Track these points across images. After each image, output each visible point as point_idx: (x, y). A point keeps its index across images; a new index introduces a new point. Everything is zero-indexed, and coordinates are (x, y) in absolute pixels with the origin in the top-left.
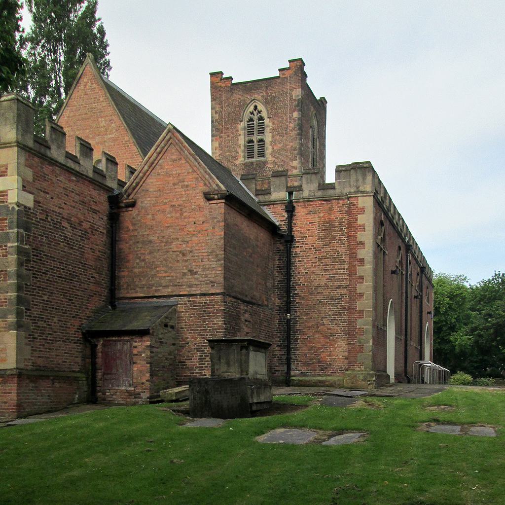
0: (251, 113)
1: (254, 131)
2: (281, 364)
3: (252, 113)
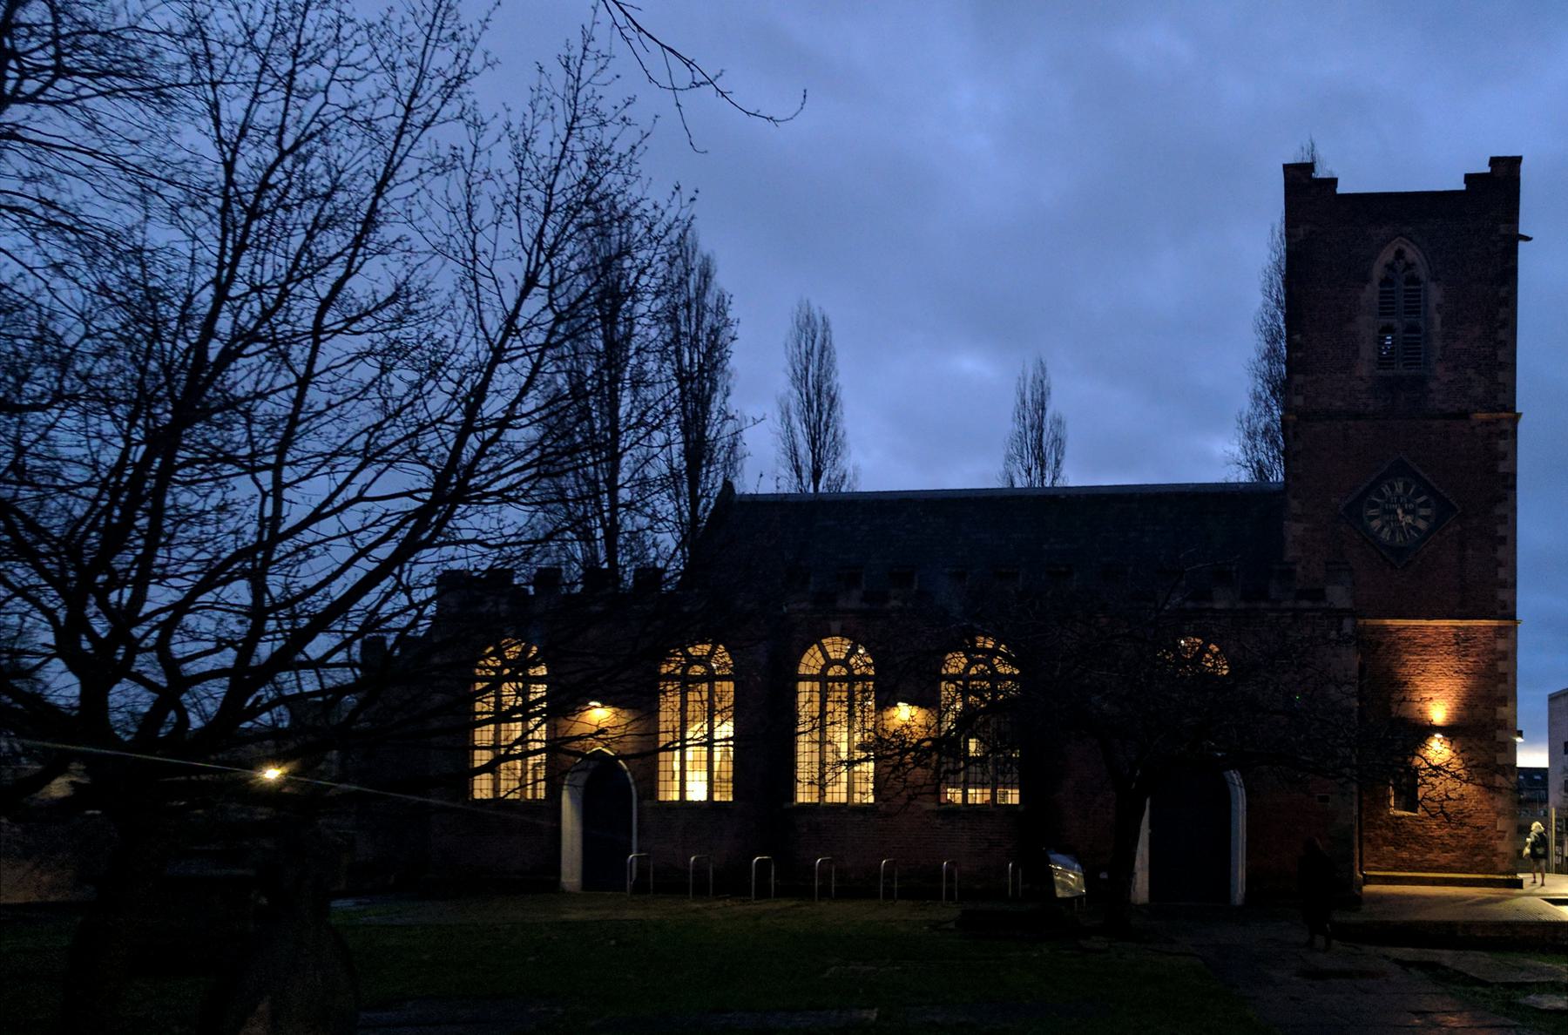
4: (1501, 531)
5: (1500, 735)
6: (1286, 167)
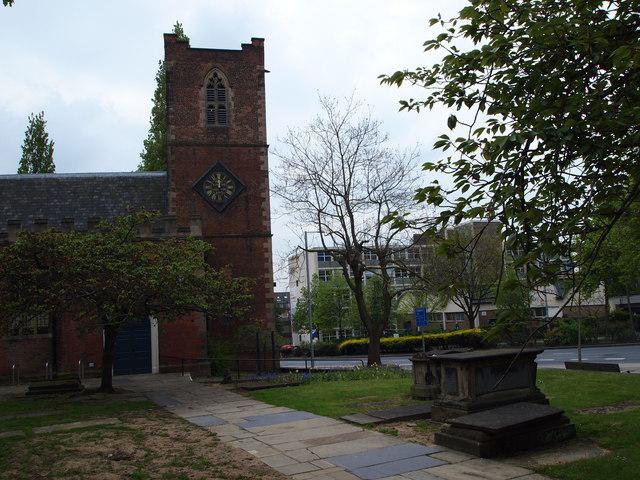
4: (263, 195)
5: (267, 286)
6: (165, 35)
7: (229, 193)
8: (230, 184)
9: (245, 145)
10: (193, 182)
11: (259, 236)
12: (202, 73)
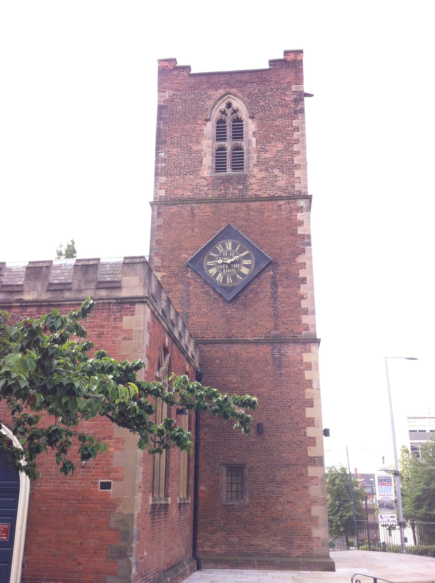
0: (221, 112)
1: (226, 160)
2: (212, 437)
3: (223, 112)
7: (245, 271)
8: (247, 257)
9: (272, 199)
10: (187, 256)
11: (296, 341)
12: (210, 103)
